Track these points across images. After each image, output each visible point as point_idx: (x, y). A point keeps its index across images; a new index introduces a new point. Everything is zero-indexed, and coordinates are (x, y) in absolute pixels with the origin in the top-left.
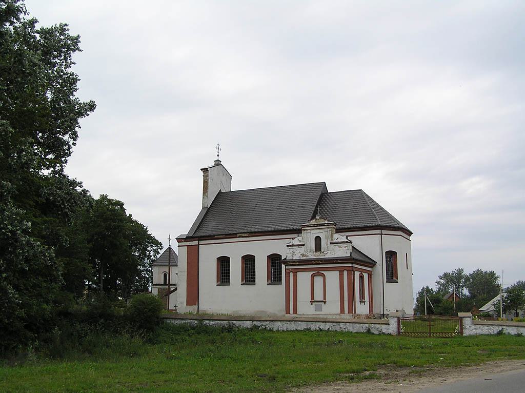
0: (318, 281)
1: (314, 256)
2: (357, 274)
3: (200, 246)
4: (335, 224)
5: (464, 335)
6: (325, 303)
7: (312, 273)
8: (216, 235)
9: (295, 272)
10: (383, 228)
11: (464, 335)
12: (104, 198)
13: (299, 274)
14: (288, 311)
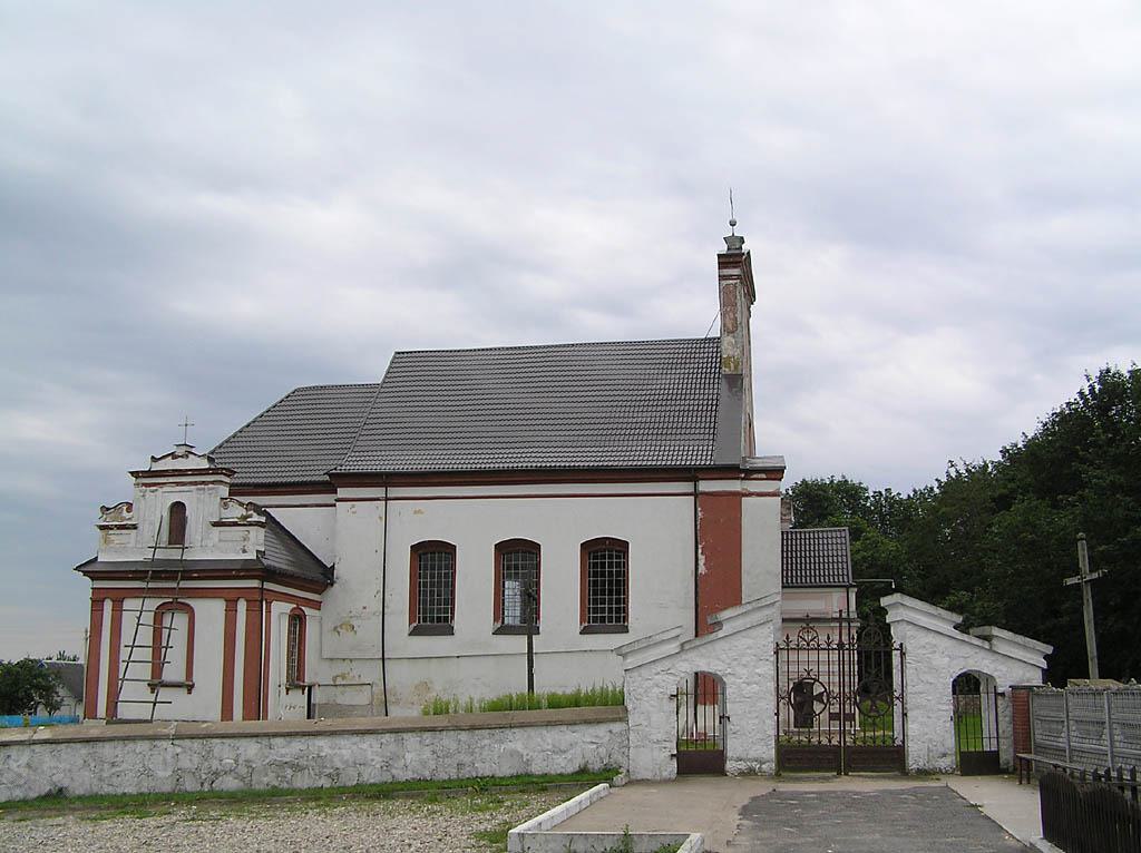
0: (180, 621)
1: (1088, 605)
2: (280, 611)
4: (230, 473)
5: (82, 661)
7: (161, 602)
8: (697, 569)
9: (119, 599)
11: (82, 661)
12: (1004, 452)
13: (129, 604)
14: (227, 712)
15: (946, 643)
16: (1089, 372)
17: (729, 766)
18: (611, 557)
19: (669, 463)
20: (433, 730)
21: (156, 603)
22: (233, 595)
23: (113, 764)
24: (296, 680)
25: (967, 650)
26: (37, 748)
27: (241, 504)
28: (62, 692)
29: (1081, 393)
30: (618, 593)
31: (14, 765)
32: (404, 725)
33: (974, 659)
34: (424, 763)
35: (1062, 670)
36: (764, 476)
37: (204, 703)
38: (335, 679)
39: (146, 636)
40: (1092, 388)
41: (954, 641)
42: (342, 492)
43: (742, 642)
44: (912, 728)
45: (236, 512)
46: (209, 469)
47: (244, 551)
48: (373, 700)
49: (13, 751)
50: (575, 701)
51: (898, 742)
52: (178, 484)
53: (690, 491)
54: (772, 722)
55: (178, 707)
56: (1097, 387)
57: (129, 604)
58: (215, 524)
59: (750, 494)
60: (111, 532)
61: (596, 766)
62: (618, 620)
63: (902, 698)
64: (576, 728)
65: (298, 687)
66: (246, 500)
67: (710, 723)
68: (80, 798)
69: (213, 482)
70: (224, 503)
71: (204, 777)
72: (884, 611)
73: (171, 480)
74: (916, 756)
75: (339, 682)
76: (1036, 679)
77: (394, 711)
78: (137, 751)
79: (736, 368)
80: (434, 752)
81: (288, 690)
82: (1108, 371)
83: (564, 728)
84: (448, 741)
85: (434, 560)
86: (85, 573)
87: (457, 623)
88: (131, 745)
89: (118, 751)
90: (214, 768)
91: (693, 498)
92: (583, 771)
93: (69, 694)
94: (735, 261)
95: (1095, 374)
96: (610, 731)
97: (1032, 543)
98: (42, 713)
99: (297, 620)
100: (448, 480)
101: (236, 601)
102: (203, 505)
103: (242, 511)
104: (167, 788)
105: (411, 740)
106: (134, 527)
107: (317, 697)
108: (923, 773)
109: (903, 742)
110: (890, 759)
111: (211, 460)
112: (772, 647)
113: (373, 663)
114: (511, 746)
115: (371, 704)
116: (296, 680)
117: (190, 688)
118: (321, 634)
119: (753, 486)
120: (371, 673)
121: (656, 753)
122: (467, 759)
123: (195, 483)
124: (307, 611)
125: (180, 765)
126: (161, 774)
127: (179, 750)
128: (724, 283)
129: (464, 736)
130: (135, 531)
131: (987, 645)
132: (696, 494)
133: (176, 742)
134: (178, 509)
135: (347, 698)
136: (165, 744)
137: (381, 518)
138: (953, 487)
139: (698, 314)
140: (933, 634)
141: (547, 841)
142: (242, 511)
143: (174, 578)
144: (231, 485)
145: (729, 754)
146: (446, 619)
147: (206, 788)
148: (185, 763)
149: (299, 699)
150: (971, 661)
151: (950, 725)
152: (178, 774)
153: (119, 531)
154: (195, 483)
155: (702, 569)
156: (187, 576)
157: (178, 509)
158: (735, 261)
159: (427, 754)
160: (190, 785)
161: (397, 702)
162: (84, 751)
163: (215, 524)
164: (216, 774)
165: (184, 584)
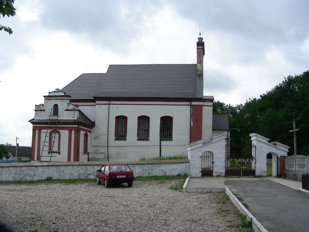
0: (57, 135)
2: (82, 133)
3: (108, 105)
6: (59, 154)
10: (192, 100)
13: (43, 131)
14: (69, 159)
15: (265, 145)
16: (285, 76)
17: (214, 174)
18: (168, 121)
19: (187, 97)
20: (142, 164)
21: (49, 131)
22: (71, 129)
23: (63, 172)
24: (86, 152)
25: (270, 147)
26: (44, 167)
27: (73, 105)
28: (10, 154)
29: (283, 82)
30: (170, 130)
31: (39, 171)
32: (135, 163)
33: (273, 150)
34: (140, 173)
35: (290, 153)
36: (208, 101)
37: (63, 157)
38: (95, 151)
39: (48, 139)
40: (286, 80)
41: (267, 145)
42: (97, 102)
43: (218, 144)
44: (257, 165)
45: (71, 107)
46: (65, 95)
47: (74, 117)
48: (105, 157)
49: (39, 168)
50: (175, 158)
51: (254, 169)
52: (56, 99)
53: (204, 107)
54: (224, 163)
55: (56, 158)
56: (287, 80)
57: (43, 131)
58: (66, 110)
59: (205, 106)
60: (38, 112)
61: (183, 174)
62: (169, 137)
63: (255, 158)
64: (177, 164)
65: (86, 153)
66: (74, 104)
67: (209, 165)
68: (56, 180)
69: (65, 99)
70: (69, 104)
71: (86, 175)
72: (250, 137)
73: (54, 98)
74: (258, 173)
75: (96, 152)
76: (286, 154)
77: (111, 160)
78: (69, 169)
79: (201, 72)
80: (143, 170)
81: (84, 154)
82: (290, 76)
83: (174, 164)
84: (146, 167)
85: (121, 120)
86: (31, 123)
87: (128, 137)
88: (67, 167)
89: (64, 168)
90: (88, 173)
91: (190, 106)
92: (179, 175)
93: (11, 154)
94: (201, 44)
95: (287, 77)
96: (186, 165)
97: (271, 120)
98: (4, 159)
99: (86, 136)
100: (123, 100)
101: (72, 130)
102: (63, 105)
103: (73, 107)
104: (77, 178)
105: (137, 167)
106: (44, 110)
107: (90, 156)
108: (259, 177)
109: (255, 169)
110: (251, 173)
111: (65, 93)
112: (225, 146)
113: (157, 146)
114: (161, 168)
115: (104, 158)
116: (86, 152)
117: (59, 153)
118: (91, 139)
119: (205, 104)
120: (104, 150)
121: (196, 171)
122: (151, 172)
123: (61, 99)
124: (88, 133)
125: (80, 172)
126: (75, 174)
127: (79, 168)
128: (198, 50)
129: (150, 166)
130: (44, 112)
131: (275, 146)
132: (191, 105)
133: (79, 167)
134: (56, 106)
135: (99, 156)
136: (76, 167)
137: (108, 109)
138: (248, 105)
139: (191, 59)
140: (262, 143)
141: (192, 189)
142: (73, 107)
143: (47, 124)
144: (70, 100)
145: (214, 171)
146: (124, 136)
147: (86, 178)
148: (81, 172)
149: (86, 156)
150: (271, 150)
151: (266, 165)
152: (79, 175)
153: (40, 112)
154: (61, 99)
155: (192, 125)
156: (59, 123)
157: (56, 106)
158: (201, 44)
159: (141, 170)
160: (82, 177)
161: (111, 158)
162: (56, 168)
163: (66, 110)
164: (89, 174)
165: (58, 126)
